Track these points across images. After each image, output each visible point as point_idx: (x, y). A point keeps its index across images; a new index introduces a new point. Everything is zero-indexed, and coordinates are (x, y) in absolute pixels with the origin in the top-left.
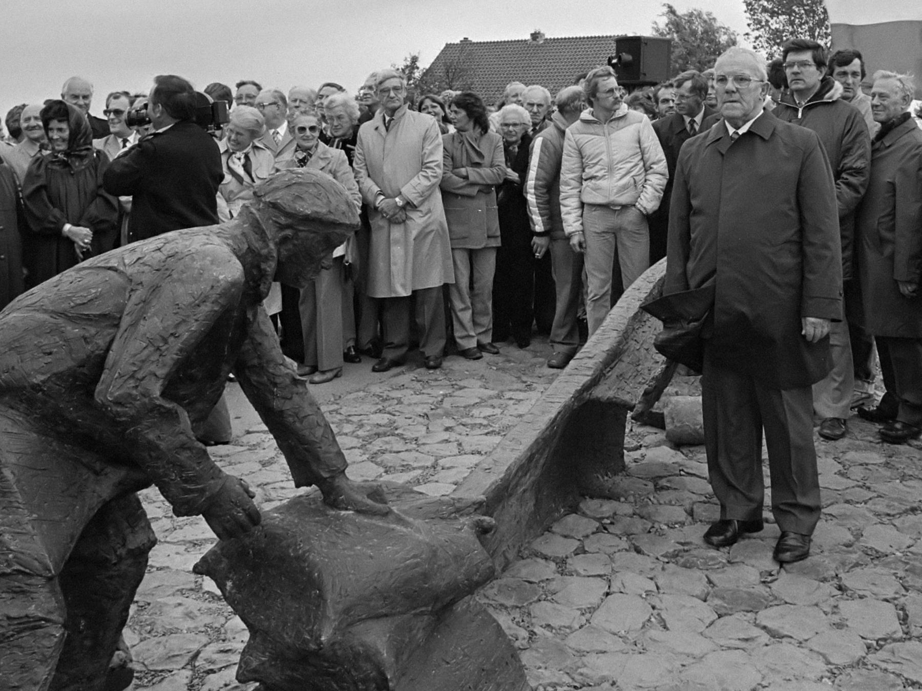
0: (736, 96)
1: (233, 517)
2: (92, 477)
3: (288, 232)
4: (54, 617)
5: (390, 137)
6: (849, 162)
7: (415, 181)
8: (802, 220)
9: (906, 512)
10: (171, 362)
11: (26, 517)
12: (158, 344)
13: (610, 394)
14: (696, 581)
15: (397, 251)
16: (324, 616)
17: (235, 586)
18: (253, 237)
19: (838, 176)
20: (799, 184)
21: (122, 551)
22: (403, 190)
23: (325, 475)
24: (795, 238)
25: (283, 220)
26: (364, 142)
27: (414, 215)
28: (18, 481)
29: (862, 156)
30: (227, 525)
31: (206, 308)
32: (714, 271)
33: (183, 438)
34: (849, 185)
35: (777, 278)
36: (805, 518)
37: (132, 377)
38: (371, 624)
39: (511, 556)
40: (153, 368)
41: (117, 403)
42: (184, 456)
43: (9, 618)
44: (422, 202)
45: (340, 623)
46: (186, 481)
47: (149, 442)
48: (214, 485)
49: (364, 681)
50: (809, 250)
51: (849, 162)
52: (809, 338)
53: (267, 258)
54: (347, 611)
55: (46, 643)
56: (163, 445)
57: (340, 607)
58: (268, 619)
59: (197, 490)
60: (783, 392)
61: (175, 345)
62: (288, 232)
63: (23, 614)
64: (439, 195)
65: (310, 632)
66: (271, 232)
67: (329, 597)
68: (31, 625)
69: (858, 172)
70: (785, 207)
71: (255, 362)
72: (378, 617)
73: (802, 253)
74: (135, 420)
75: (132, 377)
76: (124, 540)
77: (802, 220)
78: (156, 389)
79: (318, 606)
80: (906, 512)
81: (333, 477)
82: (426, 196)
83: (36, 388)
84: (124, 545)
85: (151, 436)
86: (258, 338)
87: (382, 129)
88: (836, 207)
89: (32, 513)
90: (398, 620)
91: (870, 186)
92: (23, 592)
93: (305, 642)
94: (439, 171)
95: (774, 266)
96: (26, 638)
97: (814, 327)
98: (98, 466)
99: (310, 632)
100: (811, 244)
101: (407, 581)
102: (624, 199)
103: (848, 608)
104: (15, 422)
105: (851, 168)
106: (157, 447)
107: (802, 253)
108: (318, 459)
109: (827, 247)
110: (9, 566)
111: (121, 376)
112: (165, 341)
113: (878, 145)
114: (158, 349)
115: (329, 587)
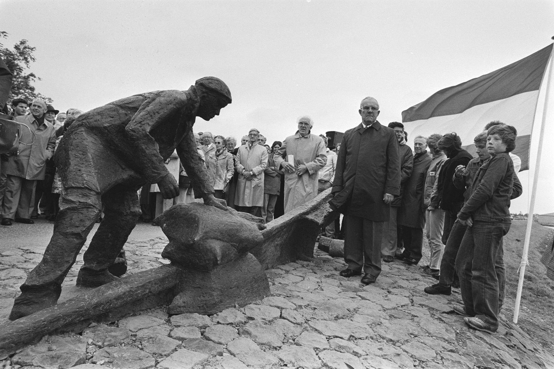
0: (372, 114)
1: (169, 187)
2: (121, 170)
3: (205, 94)
4: (97, 206)
5: (251, 151)
6: (406, 164)
7: (257, 167)
8: (388, 159)
9: (413, 279)
10: (155, 121)
11: (93, 170)
12: (151, 114)
13: (312, 218)
14: (337, 283)
15: (247, 191)
16: (198, 232)
17: (167, 225)
18: (192, 94)
19: (402, 169)
20: (388, 146)
21: (129, 211)
22: (253, 169)
23: (206, 192)
24: (385, 166)
25: (204, 90)
26: (241, 152)
27: (256, 179)
28: (93, 158)
29: (411, 163)
30: (167, 190)
31: (171, 106)
32: (355, 174)
33: (155, 152)
34: (406, 172)
35: (377, 179)
36: (376, 272)
37: (140, 123)
38: (214, 240)
39: (270, 266)
40: (148, 121)
41: (133, 131)
42: (154, 159)
43: (80, 202)
44: (258, 175)
45: (203, 236)
46: (154, 168)
47: (142, 149)
48: (163, 174)
49: (208, 260)
50: (389, 170)
51: (406, 164)
52: (385, 202)
53: (196, 102)
54: (206, 233)
55: (92, 214)
56: (147, 152)
57: (204, 231)
58: (177, 234)
59: (157, 173)
60: (374, 223)
61: (157, 116)
62: (205, 94)
63: (85, 201)
64: (263, 174)
65: (191, 238)
66: (199, 93)
67: (200, 226)
68: (87, 206)
69: (409, 168)
70: (383, 154)
71: (187, 149)
72: (218, 239)
73: (387, 171)
74: (138, 139)
75: (140, 123)
76: (130, 207)
77: (388, 159)
78: (148, 129)
79: (195, 230)
80: (413, 279)
81: (209, 194)
82: (260, 174)
83: (105, 127)
84: (129, 209)
85: (144, 147)
86: (189, 141)
87: (249, 148)
88: (400, 179)
89: (96, 170)
90: (225, 244)
91: (413, 173)
92: (87, 196)
93: (189, 241)
94: (266, 166)
95: (376, 173)
96: (85, 211)
97: (388, 197)
98: (124, 167)
99: (191, 238)
100: (391, 168)
101: (230, 230)
102: (326, 179)
103: (390, 296)
104: (96, 140)
105: (407, 167)
106: (145, 152)
107: (387, 171)
108: (204, 186)
109: (397, 170)
110: (83, 185)
111: (136, 122)
112: (154, 114)
113: (416, 160)
114: (151, 116)
115: (201, 223)
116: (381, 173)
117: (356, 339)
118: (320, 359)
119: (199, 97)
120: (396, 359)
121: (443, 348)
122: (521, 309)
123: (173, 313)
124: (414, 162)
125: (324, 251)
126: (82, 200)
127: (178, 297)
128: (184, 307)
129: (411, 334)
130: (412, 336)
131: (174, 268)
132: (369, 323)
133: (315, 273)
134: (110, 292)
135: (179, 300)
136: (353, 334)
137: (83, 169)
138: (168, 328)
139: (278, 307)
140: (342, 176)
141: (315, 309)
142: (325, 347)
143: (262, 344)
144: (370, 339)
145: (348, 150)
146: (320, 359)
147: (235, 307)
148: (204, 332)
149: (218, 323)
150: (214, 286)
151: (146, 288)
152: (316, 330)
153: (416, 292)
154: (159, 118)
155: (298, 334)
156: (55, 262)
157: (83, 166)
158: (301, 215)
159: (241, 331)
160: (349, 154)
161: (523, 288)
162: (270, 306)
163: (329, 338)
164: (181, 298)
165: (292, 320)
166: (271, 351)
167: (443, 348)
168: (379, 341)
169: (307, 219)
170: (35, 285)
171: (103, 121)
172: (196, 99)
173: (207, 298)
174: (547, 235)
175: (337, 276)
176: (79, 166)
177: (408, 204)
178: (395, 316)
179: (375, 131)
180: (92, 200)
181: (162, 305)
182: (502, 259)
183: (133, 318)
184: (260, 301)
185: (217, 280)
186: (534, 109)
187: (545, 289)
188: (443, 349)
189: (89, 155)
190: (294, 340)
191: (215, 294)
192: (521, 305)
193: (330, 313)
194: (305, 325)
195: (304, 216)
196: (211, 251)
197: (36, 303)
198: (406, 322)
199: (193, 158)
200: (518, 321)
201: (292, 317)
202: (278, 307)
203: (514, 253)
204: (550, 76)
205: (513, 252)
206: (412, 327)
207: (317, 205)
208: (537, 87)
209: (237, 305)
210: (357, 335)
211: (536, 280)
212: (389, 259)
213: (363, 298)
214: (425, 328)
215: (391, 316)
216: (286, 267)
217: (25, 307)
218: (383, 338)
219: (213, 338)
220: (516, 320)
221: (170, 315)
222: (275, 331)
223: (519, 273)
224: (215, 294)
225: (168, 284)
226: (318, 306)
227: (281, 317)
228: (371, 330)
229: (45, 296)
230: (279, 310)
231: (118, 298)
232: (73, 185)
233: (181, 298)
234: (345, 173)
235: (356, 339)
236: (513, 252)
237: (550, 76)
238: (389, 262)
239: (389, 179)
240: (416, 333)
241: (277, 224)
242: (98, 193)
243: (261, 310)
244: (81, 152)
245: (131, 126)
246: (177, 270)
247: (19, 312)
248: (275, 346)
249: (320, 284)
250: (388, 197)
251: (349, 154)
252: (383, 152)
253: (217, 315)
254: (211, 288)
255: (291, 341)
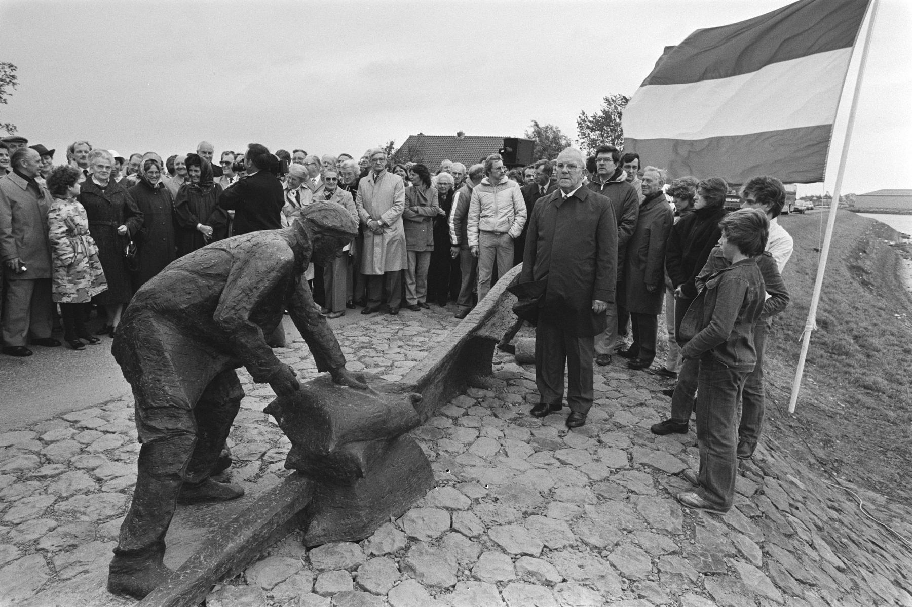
3: (319, 236)
8: (597, 247)
9: (637, 405)
11: (177, 378)
12: (247, 291)
13: (487, 334)
14: (525, 433)
18: (299, 237)
20: (598, 227)
21: (227, 399)
25: (316, 229)
28: (172, 360)
31: (273, 274)
33: (260, 342)
37: (233, 308)
38: (354, 444)
40: (244, 304)
41: (225, 321)
42: (260, 352)
43: (168, 429)
47: (242, 343)
50: (600, 263)
54: (343, 437)
55: (187, 443)
56: (249, 346)
61: (257, 293)
62: (319, 236)
63: (175, 427)
67: (334, 429)
68: (179, 433)
72: (359, 441)
73: (596, 265)
75: (233, 308)
76: (228, 393)
77: (597, 247)
80: (637, 405)
83: (182, 311)
86: (301, 292)
90: (369, 443)
92: (175, 417)
97: (599, 305)
101: (374, 424)
103: (603, 452)
104: (171, 328)
106: (246, 346)
107: (596, 265)
108: (330, 358)
109: (610, 263)
112: (251, 290)
116: (588, 268)
117: (551, 550)
118: (504, 601)
119: (310, 243)
120: (599, 584)
121: (663, 550)
122: (804, 383)
123: (311, 545)
124: (640, 211)
125: (508, 352)
126: (170, 427)
127: (315, 523)
128: (325, 535)
129: (624, 529)
130: (625, 532)
131: (304, 481)
132: (568, 519)
133: (496, 416)
134: (231, 545)
135: (317, 527)
136: (546, 544)
137: (162, 378)
138: (311, 575)
139: (447, 509)
140: (532, 272)
141: (496, 499)
142: (509, 578)
143: (431, 586)
144: (569, 549)
145: (540, 234)
146: (504, 601)
147: (390, 520)
148: (356, 576)
149: (372, 555)
150: (361, 503)
151: (273, 524)
152: (499, 546)
153: (638, 435)
154: (259, 296)
155: (475, 559)
156: (152, 515)
157: (162, 373)
158: (471, 333)
159: (403, 565)
160: (542, 239)
161: (807, 361)
162: (437, 507)
163: (515, 559)
164: (318, 525)
165: (467, 532)
166: (442, 596)
167: (663, 550)
168: (581, 549)
169: (480, 337)
170: (133, 550)
171: (178, 299)
172: (306, 245)
173: (352, 521)
174: (864, 233)
175: (527, 416)
176: (157, 374)
177: (629, 283)
178: (606, 495)
179: (578, 201)
180: (184, 423)
181: (294, 530)
182: (760, 384)
183: (262, 563)
184: (422, 500)
185: (362, 492)
186: (834, 112)
187: (843, 343)
188: (662, 553)
189: (167, 355)
190: (470, 570)
191: (363, 513)
192: (804, 376)
193: (517, 506)
194: (484, 543)
195: (474, 334)
196: (354, 460)
197: (140, 570)
198: (618, 506)
199: (309, 318)
200: (797, 407)
201: (466, 526)
202: (447, 509)
203: (807, 277)
204: (872, 21)
205: (807, 274)
206: (628, 518)
207: (494, 307)
208: (849, 42)
209: (393, 518)
210: (551, 545)
211: (834, 326)
212: (605, 360)
213: (563, 463)
214: (643, 513)
215: (599, 496)
216: (454, 411)
217: (126, 576)
218: (586, 544)
219: (369, 586)
220: (792, 409)
221: (308, 549)
222: (446, 560)
223: (802, 340)
224: (363, 513)
225: (298, 508)
226: (500, 494)
227: (452, 529)
228: (570, 534)
229: (148, 558)
230: (446, 514)
231: (241, 549)
232: (154, 405)
233: (318, 525)
234: (535, 268)
235: (551, 550)
236: (807, 274)
237: (872, 21)
238: (604, 365)
239: (600, 278)
240: (630, 527)
241: (435, 363)
242: (189, 411)
243: (424, 518)
244: (155, 352)
245: (222, 314)
246: (308, 484)
247: (120, 584)
248: (447, 586)
249: (503, 442)
250: (599, 305)
251: (542, 239)
252: (591, 236)
253: (369, 541)
254: (358, 506)
255: (467, 572)
